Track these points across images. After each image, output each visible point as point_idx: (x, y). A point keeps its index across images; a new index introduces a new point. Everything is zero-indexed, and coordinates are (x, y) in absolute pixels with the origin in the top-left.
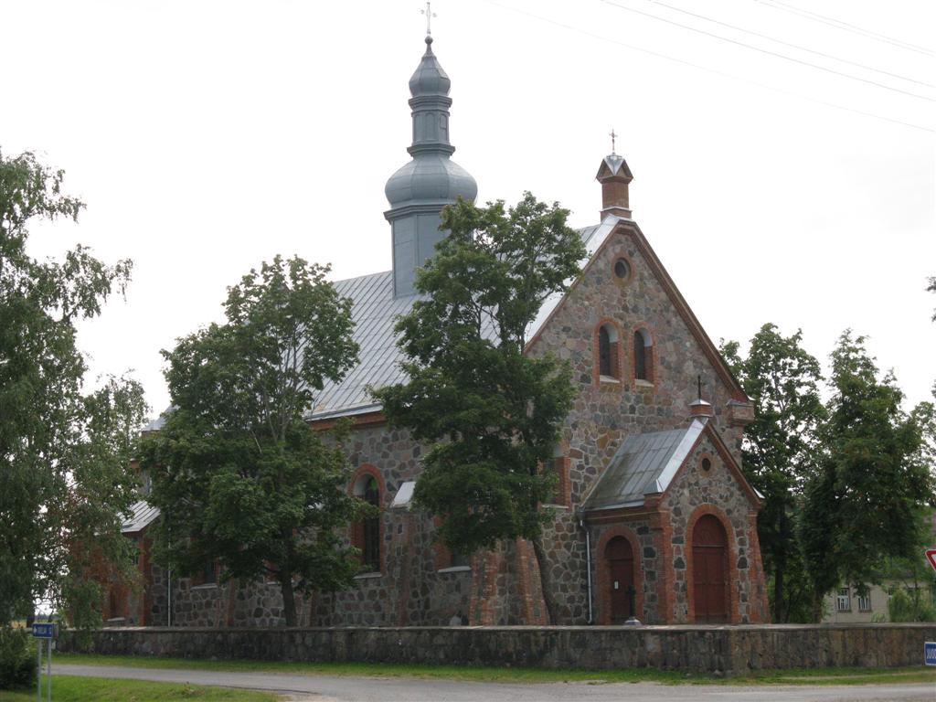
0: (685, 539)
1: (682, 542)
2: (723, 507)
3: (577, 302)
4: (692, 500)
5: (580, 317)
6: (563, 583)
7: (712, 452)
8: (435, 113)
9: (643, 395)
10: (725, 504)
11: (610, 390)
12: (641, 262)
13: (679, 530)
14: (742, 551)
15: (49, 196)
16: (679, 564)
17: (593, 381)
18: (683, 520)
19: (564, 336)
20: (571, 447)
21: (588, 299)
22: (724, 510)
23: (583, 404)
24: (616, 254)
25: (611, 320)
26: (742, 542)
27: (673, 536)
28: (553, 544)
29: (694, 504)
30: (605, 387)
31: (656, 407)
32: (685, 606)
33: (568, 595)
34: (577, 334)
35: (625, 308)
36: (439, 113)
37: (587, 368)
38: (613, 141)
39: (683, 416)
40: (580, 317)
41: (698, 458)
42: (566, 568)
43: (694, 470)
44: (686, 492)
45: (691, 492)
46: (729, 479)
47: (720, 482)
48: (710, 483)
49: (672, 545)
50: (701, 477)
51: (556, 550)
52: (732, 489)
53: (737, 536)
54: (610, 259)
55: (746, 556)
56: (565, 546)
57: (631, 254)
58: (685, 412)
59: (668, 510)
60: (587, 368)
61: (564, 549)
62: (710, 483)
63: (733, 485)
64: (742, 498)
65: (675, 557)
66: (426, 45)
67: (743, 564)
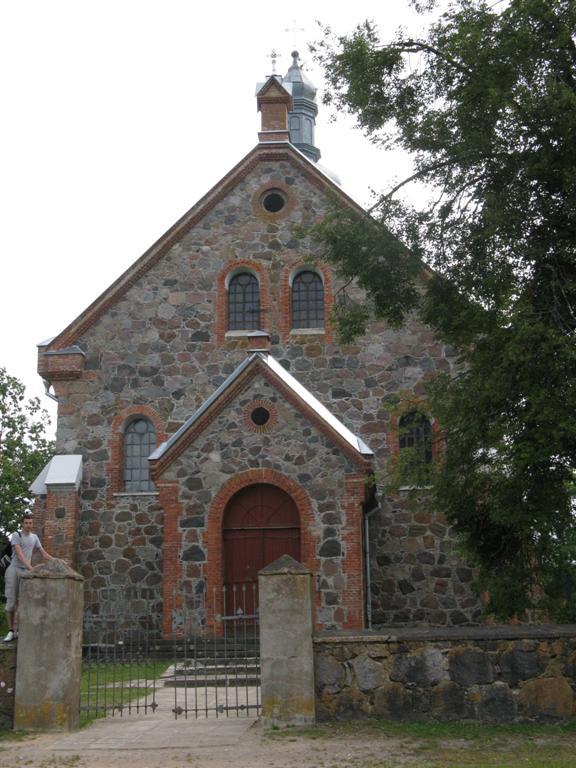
0: (206, 521)
1: (201, 525)
2: (290, 472)
3: (189, 250)
4: (224, 465)
5: (193, 266)
6: (145, 586)
7: (274, 399)
8: (300, 116)
9: (304, 347)
10: (296, 467)
11: (244, 345)
12: (306, 187)
13: (195, 509)
14: (329, 532)
15: (522, 303)
16: (194, 554)
17: (214, 338)
18: (208, 494)
19: (164, 291)
20: (170, 420)
21: (208, 243)
22: (294, 476)
23: (194, 367)
24: (262, 186)
25: (248, 263)
26: (329, 519)
27: (184, 516)
28: (130, 540)
29: (231, 471)
30: (236, 343)
31: (329, 358)
32: (201, 614)
33: (152, 603)
34: (187, 286)
35: (275, 245)
36: (304, 117)
37: (203, 324)
38: (274, 62)
39: (383, 364)
40: (193, 266)
41: (243, 409)
42: (152, 568)
43: (233, 425)
44: (215, 457)
45: (224, 456)
46: (307, 433)
47: (289, 438)
48: (266, 441)
49: (180, 529)
50: (246, 434)
51: (134, 547)
52: (312, 446)
53: (321, 511)
54: (252, 193)
55: (338, 538)
56: (152, 541)
57: (290, 181)
58: (384, 359)
59: (177, 482)
60: (203, 324)
61: (149, 546)
62: (266, 441)
63: (315, 440)
64: (333, 457)
65: (186, 545)
66: (292, 59)
67: (332, 549)
